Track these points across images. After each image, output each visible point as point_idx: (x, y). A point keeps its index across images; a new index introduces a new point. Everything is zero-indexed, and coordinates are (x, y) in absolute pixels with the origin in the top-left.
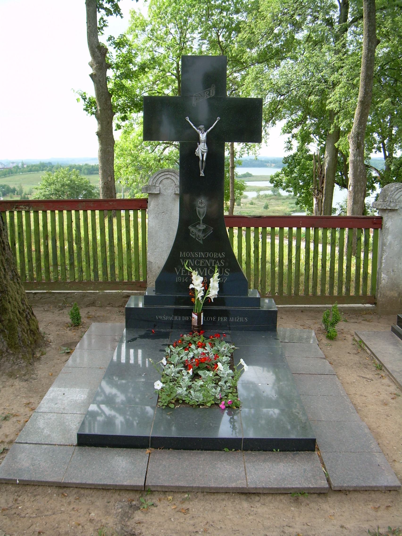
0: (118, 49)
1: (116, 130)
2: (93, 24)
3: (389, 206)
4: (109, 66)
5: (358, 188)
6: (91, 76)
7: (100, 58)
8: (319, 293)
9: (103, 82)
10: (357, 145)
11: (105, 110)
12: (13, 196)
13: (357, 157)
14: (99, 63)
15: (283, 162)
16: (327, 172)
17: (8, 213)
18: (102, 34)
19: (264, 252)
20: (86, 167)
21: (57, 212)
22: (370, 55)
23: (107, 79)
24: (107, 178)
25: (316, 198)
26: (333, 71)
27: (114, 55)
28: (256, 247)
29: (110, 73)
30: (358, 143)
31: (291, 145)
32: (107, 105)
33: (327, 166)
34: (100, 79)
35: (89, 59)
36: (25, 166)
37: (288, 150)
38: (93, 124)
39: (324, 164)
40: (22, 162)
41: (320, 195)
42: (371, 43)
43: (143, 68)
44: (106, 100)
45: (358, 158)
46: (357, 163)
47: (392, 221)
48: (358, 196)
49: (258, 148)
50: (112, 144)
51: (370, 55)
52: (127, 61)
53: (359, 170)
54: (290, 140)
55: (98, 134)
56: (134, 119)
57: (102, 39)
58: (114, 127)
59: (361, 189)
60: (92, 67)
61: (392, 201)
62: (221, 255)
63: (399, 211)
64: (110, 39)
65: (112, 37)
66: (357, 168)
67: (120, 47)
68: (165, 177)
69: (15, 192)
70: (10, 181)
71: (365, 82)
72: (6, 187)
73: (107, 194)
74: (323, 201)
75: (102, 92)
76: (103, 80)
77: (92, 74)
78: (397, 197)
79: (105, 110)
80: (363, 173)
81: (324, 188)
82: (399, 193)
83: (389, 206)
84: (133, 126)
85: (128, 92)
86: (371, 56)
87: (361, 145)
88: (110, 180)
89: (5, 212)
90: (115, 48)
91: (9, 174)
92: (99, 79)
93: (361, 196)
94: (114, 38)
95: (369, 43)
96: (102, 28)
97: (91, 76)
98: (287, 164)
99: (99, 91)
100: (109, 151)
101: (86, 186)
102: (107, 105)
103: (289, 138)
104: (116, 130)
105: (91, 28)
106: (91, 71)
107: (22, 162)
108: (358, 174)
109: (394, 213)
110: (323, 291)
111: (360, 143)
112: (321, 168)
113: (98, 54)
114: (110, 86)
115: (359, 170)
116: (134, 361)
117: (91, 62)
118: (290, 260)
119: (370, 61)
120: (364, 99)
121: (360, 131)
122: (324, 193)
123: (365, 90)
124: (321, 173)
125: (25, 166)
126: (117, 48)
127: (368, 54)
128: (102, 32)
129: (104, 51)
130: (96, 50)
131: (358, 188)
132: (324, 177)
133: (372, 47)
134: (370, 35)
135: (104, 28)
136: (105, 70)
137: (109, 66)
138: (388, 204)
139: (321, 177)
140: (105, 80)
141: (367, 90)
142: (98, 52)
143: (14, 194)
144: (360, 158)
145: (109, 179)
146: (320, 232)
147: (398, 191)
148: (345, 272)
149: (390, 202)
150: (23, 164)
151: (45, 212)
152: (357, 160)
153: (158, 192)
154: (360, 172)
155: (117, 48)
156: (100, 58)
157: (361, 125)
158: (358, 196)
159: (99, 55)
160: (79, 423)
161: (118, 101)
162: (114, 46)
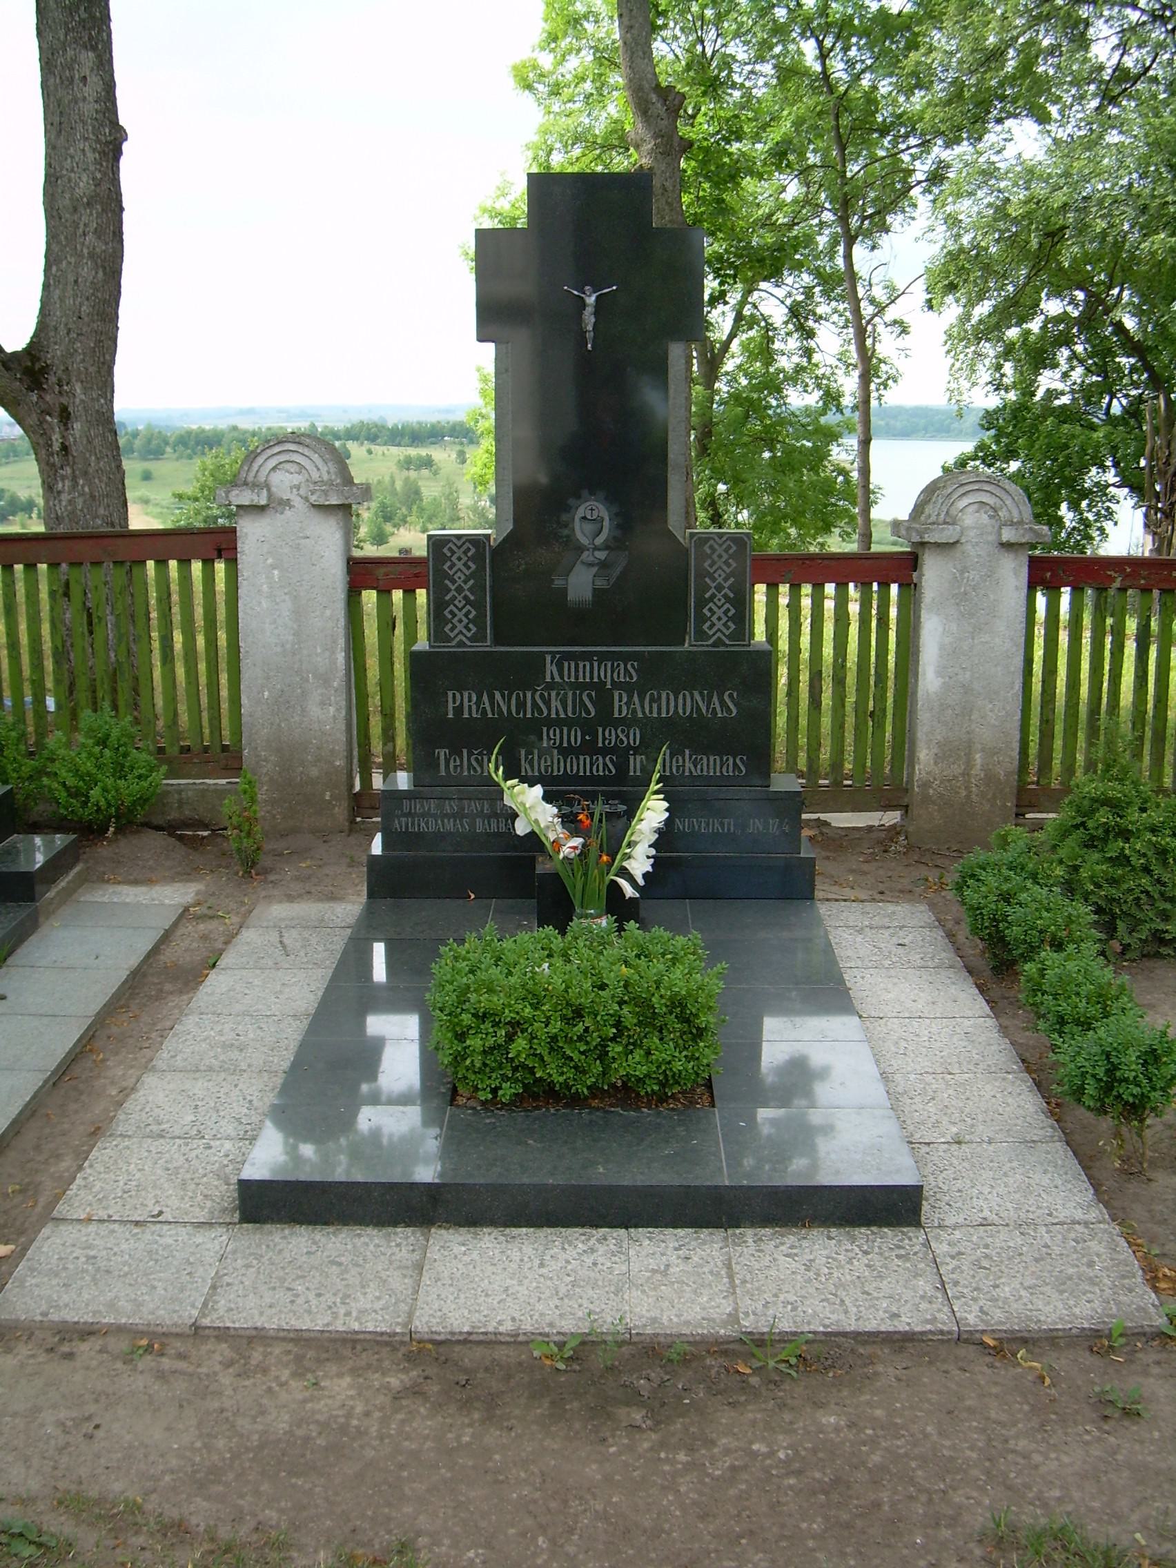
2: (641, 20)
7: (665, 122)
9: (673, 191)
12: (29, 522)
15: (982, 426)
17: (761, 589)
20: (236, 434)
21: (19, 568)
34: (667, 184)
49: (968, 385)
62: (723, 703)
69: (31, 511)
70: (12, 478)
72: (7, 495)
89: (847, 584)
91: (7, 457)
98: (992, 432)
105: (635, 31)
113: (659, 108)
116: (365, 1021)
118: (793, 719)
129: (676, 102)
130: (654, 98)
139: (1166, 473)
143: (31, 518)
148: (1058, 762)
156: (665, 122)
159: (664, 115)
160: (853, 1240)
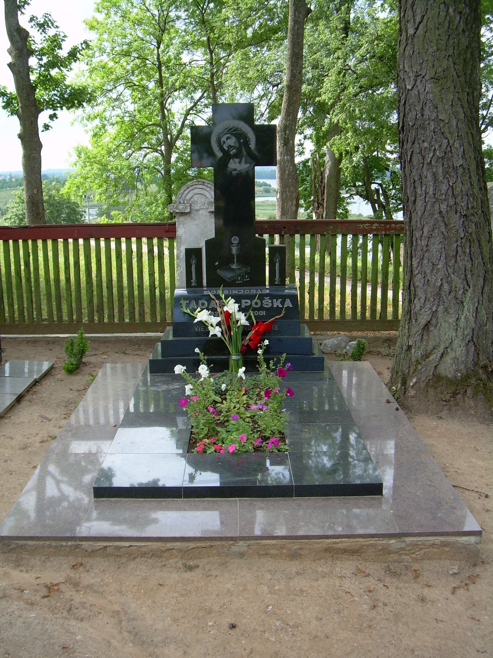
0: (43, 31)
1: (43, 131)
3: (177, 208)
4: (31, 52)
5: (287, 195)
6: (10, 65)
7: (20, 44)
8: (65, 318)
10: (284, 141)
11: (27, 107)
13: (284, 156)
14: (18, 50)
16: (327, 180)
18: (23, 13)
19: (37, 269)
22: (296, 27)
23: (29, 69)
24: (33, 190)
25: (316, 213)
26: (329, 53)
27: (38, 39)
28: (27, 264)
29: (33, 62)
30: (285, 138)
31: (303, 148)
32: (29, 100)
33: (328, 172)
35: (8, 44)
36: (14, 180)
37: (299, 154)
38: (14, 125)
39: (324, 170)
40: (10, 175)
41: (321, 209)
42: (298, 13)
43: (73, 55)
44: (28, 95)
45: (286, 157)
46: (284, 163)
47: (184, 228)
48: (287, 205)
50: (37, 148)
51: (296, 27)
52: (55, 46)
53: (287, 172)
54: (302, 142)
55: (20, 136)
56: (107, 119)
57: (23, 21)
58: (41, 127)
59: (291, 196)
60: (10, 54)
61: (182, 202)
63: (192, 215)
64: (32, 19)
65: (34, 17)
66: (285, 171)
67: (45, 28)
68: (201, 191)
71: (292, 62)
73: (32, 210)
74: (324, 216)
75: (23, 85)
76: (24, 70)
77: (10, 63)
78: (188, 197)
79: (27, 107)
80: (293, 176)
81: (325, 201)
82: (192, 192)
83: (177, 208)
84: (106, 127)
85: (55, 83)
86: (298, 29)
87: (289, 141)
88: (36, 193)
90: (38, 30)
92: (19, 68)
93: (292, 205)
94: (37, 19)
95: (295, 14)
96: (23, 6)
97: (10, 65)
99: (19, 83)
100: (34, 157)
101: (69, 202)
102: (29, 100)
103: (300, 140)
104: (43, 131)
106: (9, 59)
107: (10, 175)
108: (286, 177)
109: (186, 217)
110: (111, 316)
111: (288, 138)
112: (322, 175)
113: (18, 38)
114: (33, 77)
115: (287, 172)
117: (10, 49)
118: (68, 279)
119: (297, 35)
120: (291, 84)
121: (288, 123)
122: (325, 206)
123: (292, 71)
124: (322, 182)
125: (14, 180)
126: (41, 31)
127: (295, 26)
128: (23, 10)
129: (25, 35)
131: (287, 195)
132: (325, 187)
133: (299, 17)
134: (297, 3)
135: (26, 6)
136: (27, 58)
137: (31, 52)
138: (175, 206)
140: (26, 70)
141: (295, 71)
142: (19, 38)
144: (288, 157)
145: (35, 191)
146: (103, 244)
147: (189, 189)
149: (180, 203)
150: (11, 178)
151: (139, 240)
152: (284, 160)
153: (188, 210)
154: (289, 174)
155: (41, 31)
156: (20, 44)
157: (289, 116)
158: (287, 205)
161: (40, 93)
162: (38, 28)
